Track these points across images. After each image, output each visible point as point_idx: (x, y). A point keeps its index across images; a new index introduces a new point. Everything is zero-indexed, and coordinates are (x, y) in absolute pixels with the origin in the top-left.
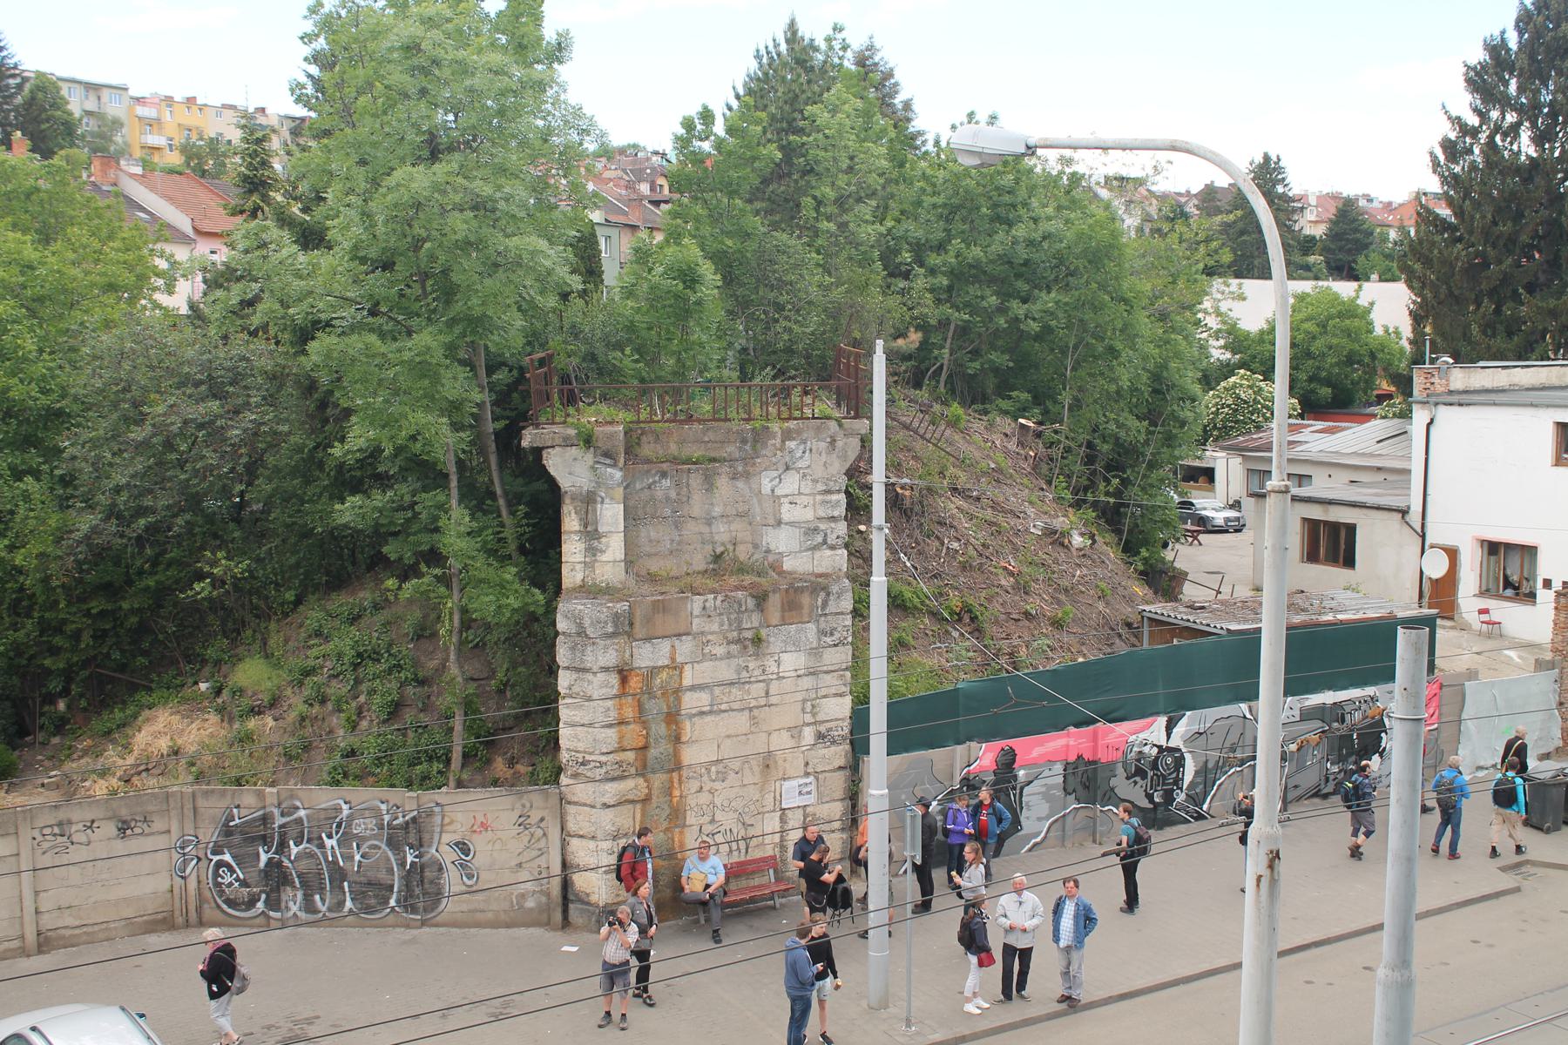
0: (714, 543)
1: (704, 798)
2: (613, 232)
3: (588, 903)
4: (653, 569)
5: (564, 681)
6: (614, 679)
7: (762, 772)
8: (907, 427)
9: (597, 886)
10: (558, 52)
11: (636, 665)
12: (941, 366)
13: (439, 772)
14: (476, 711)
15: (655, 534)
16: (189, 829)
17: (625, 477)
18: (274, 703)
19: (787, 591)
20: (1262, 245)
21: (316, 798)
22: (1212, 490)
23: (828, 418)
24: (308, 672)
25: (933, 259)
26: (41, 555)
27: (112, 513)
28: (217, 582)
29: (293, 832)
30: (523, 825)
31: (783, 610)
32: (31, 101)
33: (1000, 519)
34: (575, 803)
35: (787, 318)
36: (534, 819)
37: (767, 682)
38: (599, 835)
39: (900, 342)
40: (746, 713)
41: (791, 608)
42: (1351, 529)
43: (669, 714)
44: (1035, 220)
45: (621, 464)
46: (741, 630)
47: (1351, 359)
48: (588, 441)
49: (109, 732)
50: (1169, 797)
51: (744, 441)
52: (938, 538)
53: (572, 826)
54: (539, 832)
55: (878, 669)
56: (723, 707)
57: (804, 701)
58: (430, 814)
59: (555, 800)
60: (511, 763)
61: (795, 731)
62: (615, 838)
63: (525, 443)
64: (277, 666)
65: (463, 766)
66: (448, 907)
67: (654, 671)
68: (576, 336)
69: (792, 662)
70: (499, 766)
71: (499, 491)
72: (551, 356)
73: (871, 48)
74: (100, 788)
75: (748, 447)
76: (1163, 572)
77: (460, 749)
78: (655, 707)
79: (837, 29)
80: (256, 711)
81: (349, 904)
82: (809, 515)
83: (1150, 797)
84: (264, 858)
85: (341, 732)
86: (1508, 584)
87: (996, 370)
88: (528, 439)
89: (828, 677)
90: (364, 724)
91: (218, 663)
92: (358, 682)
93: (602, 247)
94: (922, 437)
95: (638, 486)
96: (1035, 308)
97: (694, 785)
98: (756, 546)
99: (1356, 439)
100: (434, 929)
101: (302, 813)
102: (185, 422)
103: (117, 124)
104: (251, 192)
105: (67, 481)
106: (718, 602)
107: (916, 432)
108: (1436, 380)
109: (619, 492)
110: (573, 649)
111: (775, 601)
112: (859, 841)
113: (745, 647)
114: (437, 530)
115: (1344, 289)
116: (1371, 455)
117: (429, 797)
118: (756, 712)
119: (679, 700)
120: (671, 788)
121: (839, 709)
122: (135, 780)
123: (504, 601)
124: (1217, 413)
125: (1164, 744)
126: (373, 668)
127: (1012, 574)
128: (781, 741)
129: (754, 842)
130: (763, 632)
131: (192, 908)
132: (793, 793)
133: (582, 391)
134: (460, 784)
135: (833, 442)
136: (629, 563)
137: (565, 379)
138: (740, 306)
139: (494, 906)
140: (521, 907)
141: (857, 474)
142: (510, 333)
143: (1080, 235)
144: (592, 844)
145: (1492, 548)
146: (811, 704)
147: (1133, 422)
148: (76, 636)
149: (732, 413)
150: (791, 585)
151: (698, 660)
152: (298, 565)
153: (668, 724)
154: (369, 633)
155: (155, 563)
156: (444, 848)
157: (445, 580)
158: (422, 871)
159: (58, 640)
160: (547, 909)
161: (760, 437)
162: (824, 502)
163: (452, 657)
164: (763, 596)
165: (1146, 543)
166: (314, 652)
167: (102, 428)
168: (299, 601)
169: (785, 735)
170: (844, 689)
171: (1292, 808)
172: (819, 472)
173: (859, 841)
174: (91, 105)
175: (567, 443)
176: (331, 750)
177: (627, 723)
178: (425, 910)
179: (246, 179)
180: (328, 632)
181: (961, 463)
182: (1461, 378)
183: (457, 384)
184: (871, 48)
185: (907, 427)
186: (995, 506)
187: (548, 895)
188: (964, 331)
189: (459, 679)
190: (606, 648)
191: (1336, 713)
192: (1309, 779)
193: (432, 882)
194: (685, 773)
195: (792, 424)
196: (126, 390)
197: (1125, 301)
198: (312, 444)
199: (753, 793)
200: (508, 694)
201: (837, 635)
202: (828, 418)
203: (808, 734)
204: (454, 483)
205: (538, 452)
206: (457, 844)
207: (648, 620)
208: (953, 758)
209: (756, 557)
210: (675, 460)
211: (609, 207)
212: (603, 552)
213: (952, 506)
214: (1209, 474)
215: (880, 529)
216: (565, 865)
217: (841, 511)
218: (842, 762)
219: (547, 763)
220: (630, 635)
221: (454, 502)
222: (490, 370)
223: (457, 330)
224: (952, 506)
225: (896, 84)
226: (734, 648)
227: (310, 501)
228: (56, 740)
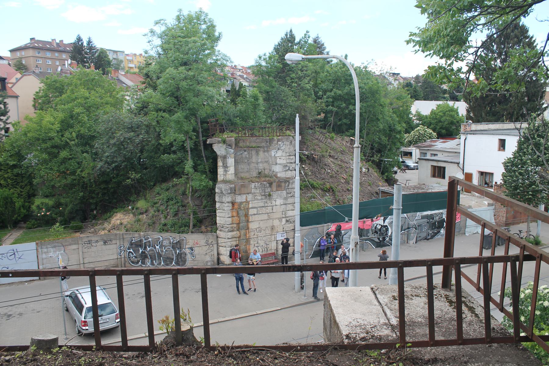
4: (242, 176)
5: (218, 205)
6: (230, 205)
8: (317, 139)
10: (218, 39)
16: (122, 243)
18: (146, 211)
20: (352, 79)
21: (153, 236)
22: (411, 158)
24: (155, 203)
25: (328, 94)
26: (88, 173)
27: (106, 162)
28: (133, 180)
29: (148, 244)
32: (99, 56)
33: (342, 164)
35: (283, 110)
36: (210, 242)
41: (279, 187)
42: (444, 168)
43: (245, 215)
45: (234, 147)
46: (265, 192)
47: (452, 123)
48: (224, 142)
49: (106, 219)
50: (384, 239)
51: (267, 142)
63: (208, 143)
64: (148, 202)
67: (241, 203)
68: (226, 114)
70: (203, 228)
73: (318, 37)
74: (103, 233)
76: (392, 179)
78: (242, 213)
79: (307, 32)
80: (142, 213)
81: (162, 263)
82: (285, 162)
83: (379, 239)
84: (141, 251)
85: (163, 219)
86: (486, 183)
87: (346, 124)
90: (169, 217)
91: (134, 201)
92: (167, 206)
97: (253, 233)
98: (270, 170)
99: (450, 144)
101: (150, 239)
102: (125, 138)
103: (122, 61)
105: (96, 154)
108: (467, 127)
110: (219, 197)
111: (274, 185)
115: (451, 103)
116: (455, 149)
117: (185, 235)
120: (246, 234)
122: (111, 231)
124: (414, 137)
125: (382, 224)
126: (171, 202)
127: (344, 179)
128: (276, 223)
130: (271, 193)
131: (123, 263)
134: (192, 232)
136: (236, 174)
137: (222, 126)
143: (370, 88)
144: (225, 249)
145: (482, 173)
147: (383, 138)
148: (98, 194)
151: (253, 200)
152: (154, 176)
154: (171, 193)
155: (117, 175)
159: (93, 195)
161: (271, 141)
164: (272, 183)
165: (387, 172)
166: (157, 198)
167: (104, 140)
168: (154, 185)
169: (277, 220)
171: (418, 243)
172: (287, 150)
174: (115, 57)
175: (219, 142)
176: (160, 224)
180: (160, 193)
181: (333, 149)
182: (474, 127)
184: (318, 37)
186: (341, 161)
187: (214, 262)
188: (337, 113)
191: (431, 217)
192: (424, 235)
195: (280, 137)
196: (110, 130)
197: (381, 105)
198: (157, 144)
203: (284, 220)
205: (211, 145)
207: (240, 189)
210: (248, 147)
213: (329, 161)
214: (411, 154)
216: (218, 254)
220: (235, 193)
224: (329, 161)
226: (263, 197)
227: (156, 159)
228: (94, 221)
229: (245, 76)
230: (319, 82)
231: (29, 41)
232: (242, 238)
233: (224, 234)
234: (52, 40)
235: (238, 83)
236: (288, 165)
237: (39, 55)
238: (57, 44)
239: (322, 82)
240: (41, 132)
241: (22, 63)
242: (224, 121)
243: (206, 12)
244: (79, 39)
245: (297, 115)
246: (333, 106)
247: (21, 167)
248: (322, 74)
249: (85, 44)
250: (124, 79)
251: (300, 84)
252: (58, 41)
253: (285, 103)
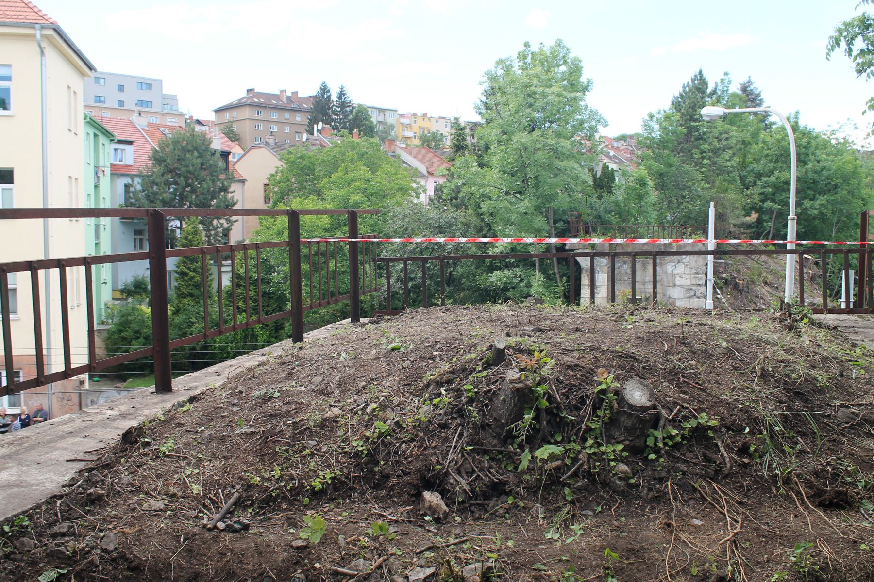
10: (586, 89)
12: (769, 232)
25: (764, 179)
39: (748, 218)
44: (818, 162)
73: (749, 82)
82: (688, 283)
96: (817, 204)
98: (664, 295)
104: (457, 151)
142: (562, 201)
143: (839, 168)
172: (693, 264)
174: (381, 119)
179: (456, 145)
184: (749, 82)
222: (555, 222)
224: (764, 290)
225: (761, 100)
229: (612, 153)
230: (749, 158)
231: (244, 94)
234: (281, 91)
235: (601, 165)
236: (694, 288)
237: (260, 117)
238: (289, 98)
240: (442, 192)
241: (232, 131)
243: (568, 46)
244: (325, 89)
245: (712, 203)
246: (773, 201)
247: (268, 283)
248: (754, 146)
249: (334, 98)
250: (405, 156)
252: (289, 94)
253: (691, 191)
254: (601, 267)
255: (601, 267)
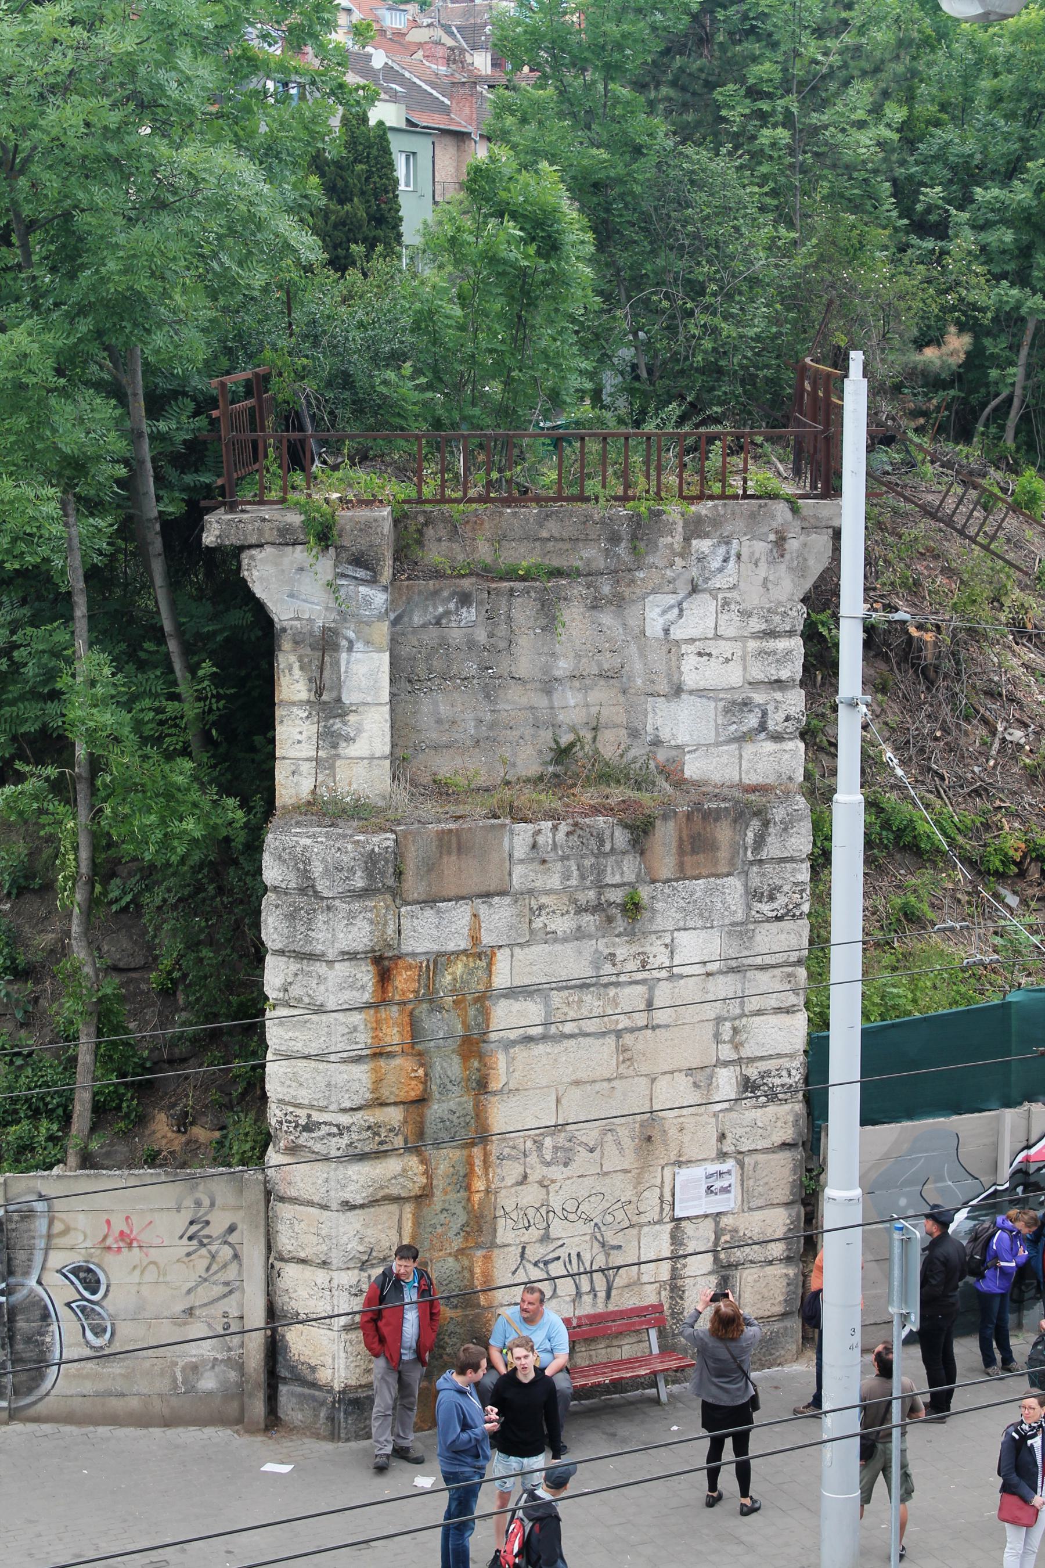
0: (556, 726)
1: (531, 1195)
2: (422, 146)
3: (314, 1385)
5: (275, 975)
6: (366, 974)
7: (638, 1150)
8: (931, 513)
9: (329, 1353)
11: (406, 948)
12: (1009, 400)
13: (51, 1138)
14: (116, 1030)
15: (444, 707)
17: (393, 603)
19: (689, 816)
23: (774, 496)
30: (197, 1235)
31: (681, 852)
34: (293, 1200)
36: (217, 1228)
37: (651, 984)
38: (336, 1261)
39: (930, 353)
40: (611, 1040)
41: (696, 846)
45: (386, 574)
46: (601, 887)
48: (324, 535)
51: (614, 539)
52: (985, 721)
53: (285, 1242)
54: (226, 1252)
55: (846, 962)
56: (569, 1028)
57: (719, 1020)
58: (28, 1215)
59: (256, 1194)
60: (183, 1123)
61: (701, 1075)
62: (363, 1266)
63: (209, 539)
65: (93, 1129)
66: (60, 1385)
67: (439, 960)
69: (697, 946)
70: (162, 1128)
71: (168, 626)
72: (266, 378)
75: (622, 549)
77: (87, 1096)
78: (442, 1026)
82: (733, 675)
88: (214, 531)
89: (760, 975)
93: (401, 172)
94: (961, 533)
95: (417, 619)
97: (511, 1171)
98: (634, 733)
100: (31, 1427)
106: (561, 835)
107: (949, 522)
109: (382, 631)
110: (291, 917)
112: (813, 1286)
113: (610, 920)
114: (55, 695)
118: (628, 1039)
119: (485, 1014)
120: (469, 1175)
121: (790, 1034)
123: (175, 827)
128: (676, 1091)
129: (622, 1278)
130: (644, 893)
132: (694, 1191)
133: (323, 442)
134: (87, 1161)
135: (781, 541)
136: (400, 761)
137: (291, 420)
138: (621, 284)
139: (143, 1386)
140: (191, 1390)
141: (823, 597)
142: (182, 338)
144: (321, 1276)
146: (731, 1027)
149: (592, 486)
150: (698, 806)
151: (520, 937)
153: (465, 1057)
156: (53, 1279)
157: (60, 788)
158: (12, 1320)
160: (238, 1393)
161: (642, 532)
162: (762, 653)
163: (76, 929)
164: (641, 821)
169: (683, 1082)
170: (792, 999)
173: (813, 1286)
175: (287, 539)
177: (390, 1055)
178: (16, 1392)
183: (87, 424)
185: (931, 513)
187: (240, 1367)
189: (88, 970)
190: (351, 916)
193: (28, 1340)
194: (494, 1148)
195: (704, 508)
199: (621, 1188)
200: (181, 999)
201: (781, 900)
202: (774, 496)
203: (726, 1082)
204: (81, 611)
206: (75, 1271)
207: (430, 867)
208: (998, 1133)
209: (633, 753)
210: (486, 573)
211: (414, 98)
212: (349, 739)
215: (853, 704)
216: (272, 1312)
217: (794, 669)
218: (787, 1134)
219: (247, 1124)
220: (395, 893)
221: (80, 644)
222: (157, 404)
223: (84, 326)
226: (589, 921)
232: (438, 1199)
233: (320, 1170)
236: (759, 698)
239: (943, 107)
242: (310, 386)
251: (815, 130)
253: (722, 259)
254: (363, 623)
255: (363, 623)
